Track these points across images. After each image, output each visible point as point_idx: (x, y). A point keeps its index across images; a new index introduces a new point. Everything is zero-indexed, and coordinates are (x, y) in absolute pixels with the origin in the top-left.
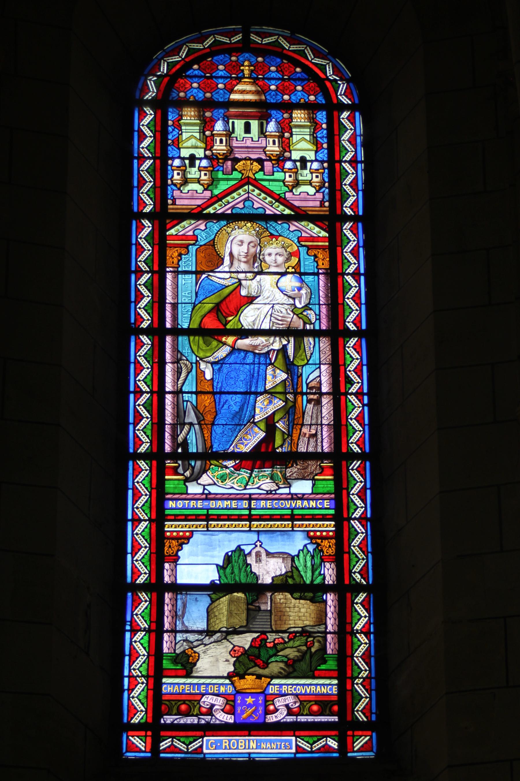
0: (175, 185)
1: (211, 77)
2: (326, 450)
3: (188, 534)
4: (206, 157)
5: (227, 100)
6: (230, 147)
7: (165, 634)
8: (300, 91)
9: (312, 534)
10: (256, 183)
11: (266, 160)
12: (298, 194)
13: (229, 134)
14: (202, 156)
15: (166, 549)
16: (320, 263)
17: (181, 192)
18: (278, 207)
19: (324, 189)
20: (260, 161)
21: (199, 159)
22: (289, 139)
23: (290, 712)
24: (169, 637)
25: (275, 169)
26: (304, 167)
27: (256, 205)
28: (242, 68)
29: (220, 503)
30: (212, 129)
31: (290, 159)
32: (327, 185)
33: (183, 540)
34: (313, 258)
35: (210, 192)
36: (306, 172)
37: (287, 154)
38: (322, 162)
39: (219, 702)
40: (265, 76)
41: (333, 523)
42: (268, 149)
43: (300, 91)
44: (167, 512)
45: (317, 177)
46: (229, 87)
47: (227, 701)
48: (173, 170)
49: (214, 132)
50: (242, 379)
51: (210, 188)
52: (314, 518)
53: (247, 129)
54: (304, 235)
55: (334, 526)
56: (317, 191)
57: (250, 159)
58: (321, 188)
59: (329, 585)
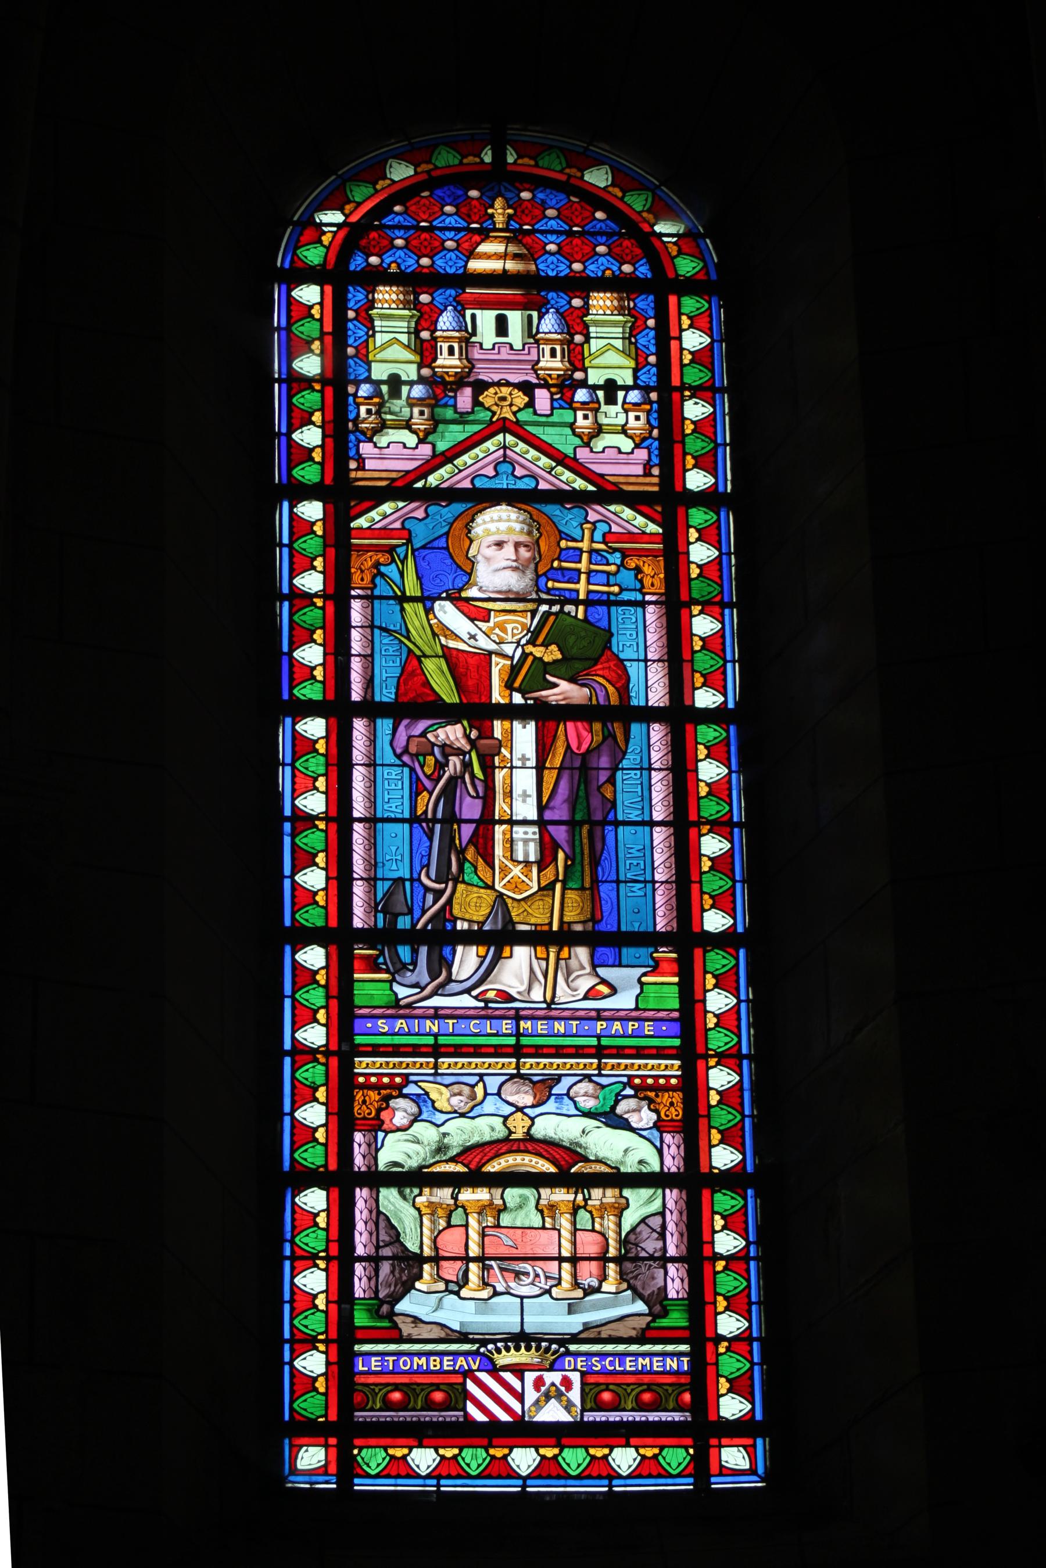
0: (363, 433)
1: (431, 229)
6: (467, 358)
9: (637, 1081)
13: (467, 338)
14: (414, 377)
19: (650, 441)
20: (527, 388)
25: (556, 404)
26: (395, 393)
27: (519, 472)
31: (583, 384)
32: (655, 432)
35: (430, 446)
37: (579, 375)
38: (646, 389)
42: (541, 364)
49: (438, 334)
51: (430, 438)
53: (502, 326)
57: (508, 384)
58: (644, 439)
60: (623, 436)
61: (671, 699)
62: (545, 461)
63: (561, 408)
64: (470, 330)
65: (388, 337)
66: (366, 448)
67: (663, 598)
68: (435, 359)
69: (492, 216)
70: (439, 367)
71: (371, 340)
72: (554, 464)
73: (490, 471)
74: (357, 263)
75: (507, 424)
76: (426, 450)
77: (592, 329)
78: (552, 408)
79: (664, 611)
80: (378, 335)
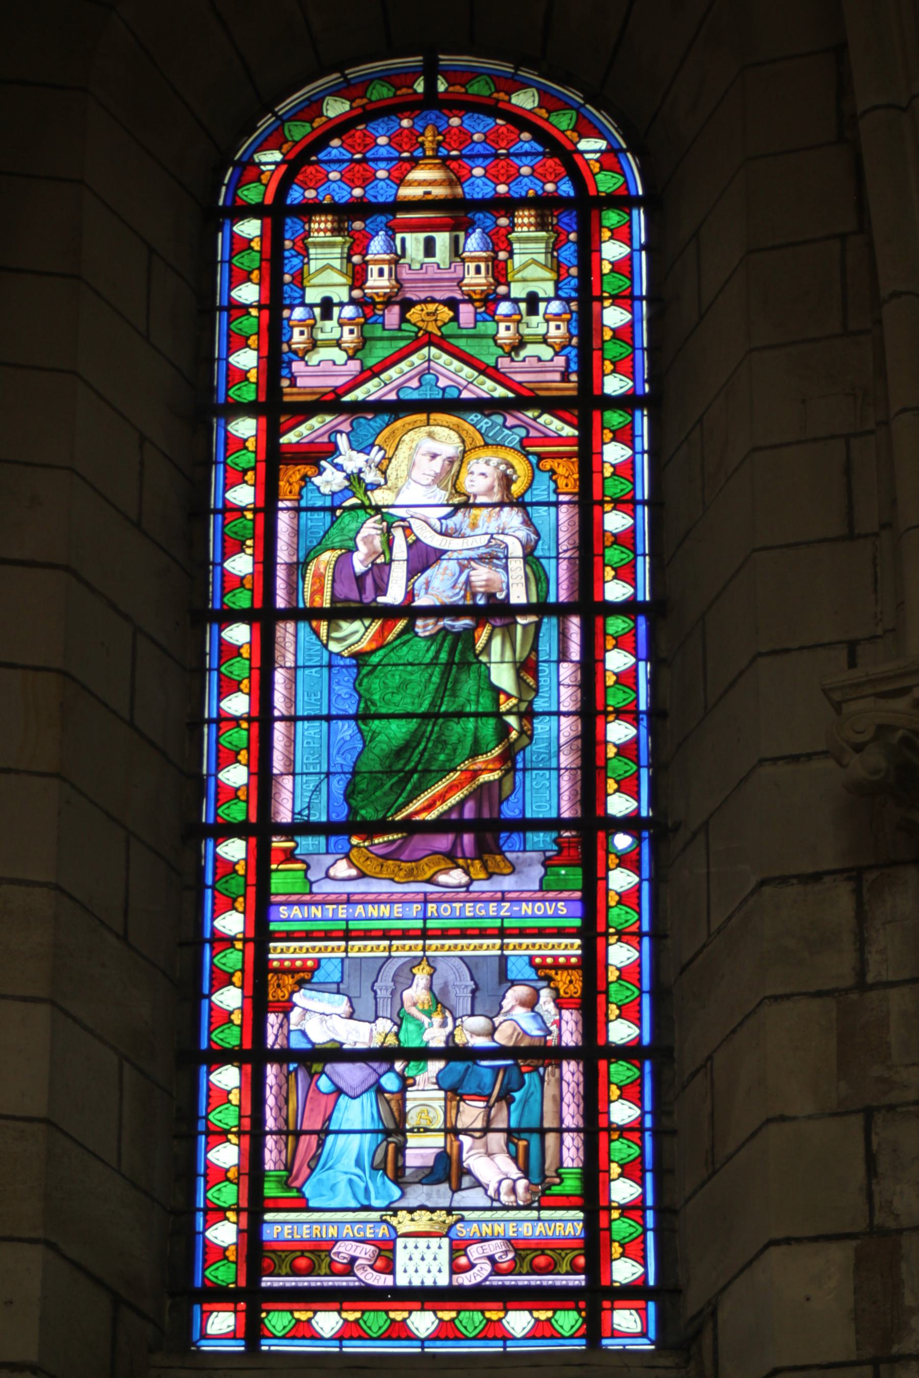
0: (295, 352)
1: (364, 160)
2: (566, 815)
3: (310, 963)
4: (353, 301)
5: (391, 199)
6: (397, 280)
7: (268, 1137)
8: (527, 176)
9: (538, 960)
10: (442, 343)
11: (464, 301)
12: (520, 358)
13: (397, 259)
14: (346, 299)
15: (271, 990)
16: (561, 482)
17: (307, 365)
18: (483, 383)
19: (568, 349)
20: (452, 304)
21: (543, 300)
22: (506, 261)
23: (496, 1270)
24: (276, 1142)
25: (479, 317)
26: (533, 310)
27: (443, 383)
28: (420, 139)
29: (372, 911)
30: (364, 252)
31: (506, 297)
32: (574, 341)
33: (302, 974)
34: (547, 475)
35: (358, 362)
36: (539, 319)
37: (502, 290)
38: (568, 300)
39: (364, 1252)
40: (512, 150)
41: (578, 942)
42: (465, 281)
43: (527, 176)
44: (273, 927)
45: (558, 327)
46: (396, 174)
47: (380, 1250)
48: (292, 327)
49: (368, 258)
50: (415, 692)
51: (359, 355)
52: (541, 933)
53: (429, 248)
54: (533, 433)
55: (580, 947)
56: (350, 358)
57: (433, 301)
58: (564, 347)
59: (567, 1048)
60: (337, 349)
61: (580, 595)
62: (467, 371)
63: (485, 320)
64: (399, 252)
65: (321, 263)
66: (297, 366)
67: (576, 498)
68: (366, 280)
69: (422, 145)
70: (466, 285)
71: (306, 267)
72: (476, 374)
73: (415, 383)
74: (296, 195)
75: (433, 339)
76: (354, 366)
77: (516, 246)
78: (476, 321)
79: (577, 510)
80: (312, 262)
